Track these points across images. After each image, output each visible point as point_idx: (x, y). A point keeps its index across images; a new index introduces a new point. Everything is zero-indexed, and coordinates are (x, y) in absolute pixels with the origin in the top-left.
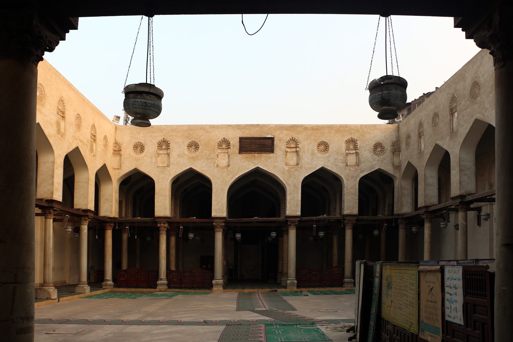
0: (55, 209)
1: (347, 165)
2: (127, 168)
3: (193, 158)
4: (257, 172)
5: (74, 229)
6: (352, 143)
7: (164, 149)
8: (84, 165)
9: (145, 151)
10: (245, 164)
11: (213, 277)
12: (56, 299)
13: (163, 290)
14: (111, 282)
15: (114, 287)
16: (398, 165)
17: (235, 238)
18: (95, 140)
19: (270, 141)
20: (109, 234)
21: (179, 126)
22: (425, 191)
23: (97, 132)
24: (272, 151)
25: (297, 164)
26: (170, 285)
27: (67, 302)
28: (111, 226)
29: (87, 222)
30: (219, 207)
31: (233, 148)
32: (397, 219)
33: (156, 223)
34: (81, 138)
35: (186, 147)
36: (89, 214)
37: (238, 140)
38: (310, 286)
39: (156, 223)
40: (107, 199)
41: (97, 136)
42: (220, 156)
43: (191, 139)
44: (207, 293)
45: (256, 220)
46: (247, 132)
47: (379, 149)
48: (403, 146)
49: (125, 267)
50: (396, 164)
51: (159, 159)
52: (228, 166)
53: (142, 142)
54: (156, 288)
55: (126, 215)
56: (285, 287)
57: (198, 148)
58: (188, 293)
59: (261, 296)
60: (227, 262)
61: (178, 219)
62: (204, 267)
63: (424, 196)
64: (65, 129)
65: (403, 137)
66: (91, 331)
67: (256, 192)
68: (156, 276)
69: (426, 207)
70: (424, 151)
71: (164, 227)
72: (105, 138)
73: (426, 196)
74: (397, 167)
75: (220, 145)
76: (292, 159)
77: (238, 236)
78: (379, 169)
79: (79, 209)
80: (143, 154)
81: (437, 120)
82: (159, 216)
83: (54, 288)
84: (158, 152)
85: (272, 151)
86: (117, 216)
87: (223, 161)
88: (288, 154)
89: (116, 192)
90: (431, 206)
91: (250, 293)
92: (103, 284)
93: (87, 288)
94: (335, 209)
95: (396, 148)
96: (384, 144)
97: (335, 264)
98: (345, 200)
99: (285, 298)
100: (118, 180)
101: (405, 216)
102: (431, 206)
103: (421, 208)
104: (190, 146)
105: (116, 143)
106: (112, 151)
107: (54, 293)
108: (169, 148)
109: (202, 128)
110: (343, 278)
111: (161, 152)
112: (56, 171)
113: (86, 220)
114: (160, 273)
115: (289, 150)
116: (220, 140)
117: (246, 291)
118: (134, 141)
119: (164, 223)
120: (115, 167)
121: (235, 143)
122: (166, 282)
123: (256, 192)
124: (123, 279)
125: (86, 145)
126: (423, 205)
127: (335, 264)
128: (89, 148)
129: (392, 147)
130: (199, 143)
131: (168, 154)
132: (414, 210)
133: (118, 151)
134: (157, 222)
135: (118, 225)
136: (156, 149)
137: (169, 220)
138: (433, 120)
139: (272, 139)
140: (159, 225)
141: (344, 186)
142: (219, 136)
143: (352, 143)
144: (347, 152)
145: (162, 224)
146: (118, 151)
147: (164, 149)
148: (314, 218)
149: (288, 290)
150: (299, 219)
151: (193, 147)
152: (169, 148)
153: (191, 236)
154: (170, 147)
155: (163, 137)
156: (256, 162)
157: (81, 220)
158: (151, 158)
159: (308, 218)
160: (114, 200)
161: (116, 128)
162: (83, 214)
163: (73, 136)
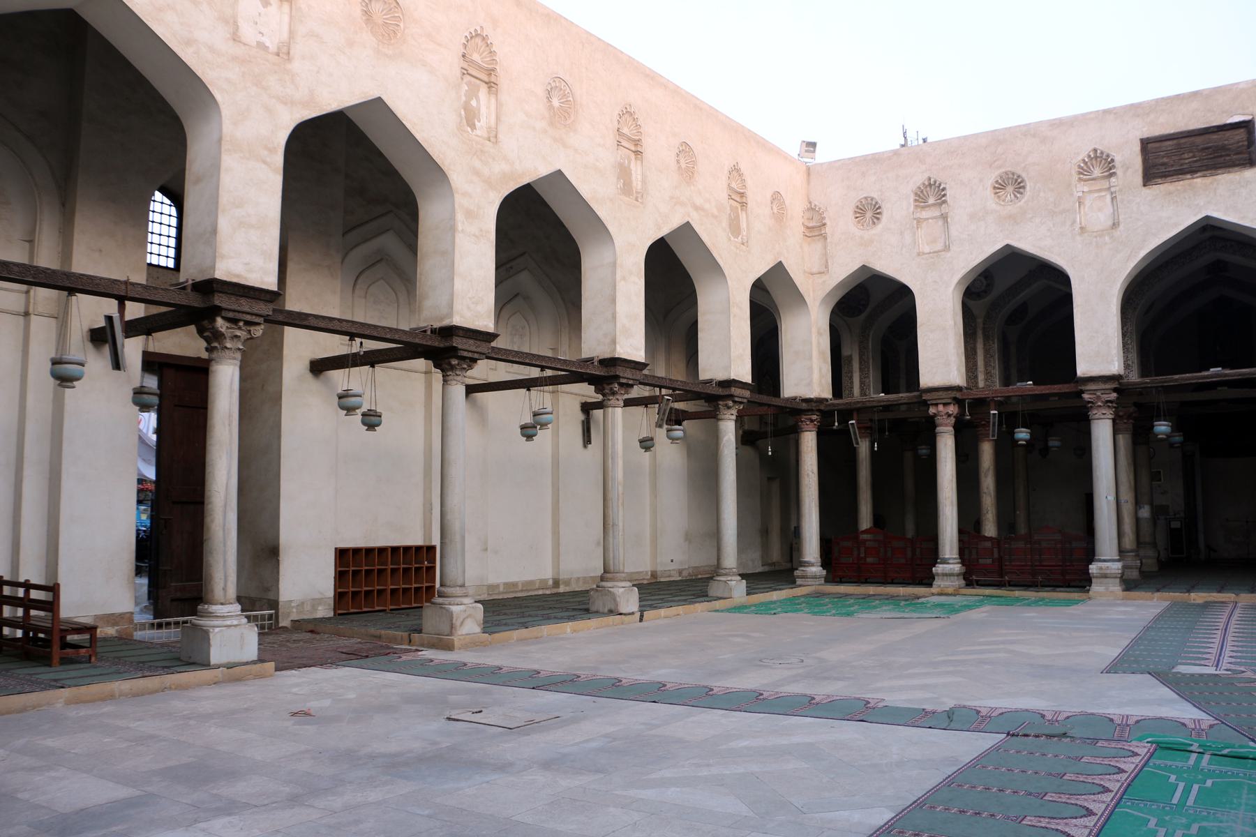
0: (624, 381)
2: (843, 268)
4: (1209, 236)
5: (743, 436)
7: (933, 205)
8: (798, 298)
9: (884, 218)
11: (1090, 554)
12: (633, 613)
13: (950, 590)
14: (817, 570)
15: (828, 580)
18: (744, 205)
19: (1241, 134)
20: (809, 442)
21: (966, 138)
23: (749, 183)
26: (973, 575)
27: (666, 621)
28: (812, 421)
29: (734, 412)
30: (1100, 345)
31: (1125, 173)
33: (926, 404)
34: (699, 201)
35: (989, 192)
36: (735, 391)
39: (926, 404)
41: (749, 194)
42: (1087, 203)
43: (1000, 167)
44: (1069, 603)
45: (1216, 375)
46: (1162, 120)
51: (920, 233)
52: (1115, 225)
53: (875, 195)
54: (930, 585)
55: (863, 393)
57: (1024, 187)
58: (1053, 603)
64: (644, 182)
66: (555, 721)
68: (933, 555)
71: (945, 416)
72: (776, 197)
75: (1084, 171)
79: (709, 382)
80: (880, 227)
84: (918, 215)
86: (827, 393)
87: (1097, 212)
89: (820, 334)
91: (1206, 605)
92: (797, 573)
93: (739, 588)
104: (999, 187)
105: (811, 208)
106: (803, 229)
107: (629, 600)
108: (945, 202)
109: (1029, 132)
111: (925, 214)
112: (621, 287)
113: (729, 408)
114: (941, 542)
116: (1083, 155)
117: (1198, 597)
118: (854, 198)
119: (945, 404)
120: (815, 270)
121: (1130, 160)
122: (957, 568)
125: (715, 217)
128: (725, 224)
130: (1024, 175)
131: (944, 217)
133: (816, 229)
134: (925, 401)
135: (833, 420)
136: (912, 208)
137: (958, 395)
140: (932, 410)
145: (941, 408)
146: (816, 229)
151: (1010, 189)
152: (945, 202)
154: (948, 198)
155: (926, 175)
157: (717, 409)
158: (902, 233)
160: (815, 353)
161: (809, 171)
162: (720, 391)
163: (672, 198)
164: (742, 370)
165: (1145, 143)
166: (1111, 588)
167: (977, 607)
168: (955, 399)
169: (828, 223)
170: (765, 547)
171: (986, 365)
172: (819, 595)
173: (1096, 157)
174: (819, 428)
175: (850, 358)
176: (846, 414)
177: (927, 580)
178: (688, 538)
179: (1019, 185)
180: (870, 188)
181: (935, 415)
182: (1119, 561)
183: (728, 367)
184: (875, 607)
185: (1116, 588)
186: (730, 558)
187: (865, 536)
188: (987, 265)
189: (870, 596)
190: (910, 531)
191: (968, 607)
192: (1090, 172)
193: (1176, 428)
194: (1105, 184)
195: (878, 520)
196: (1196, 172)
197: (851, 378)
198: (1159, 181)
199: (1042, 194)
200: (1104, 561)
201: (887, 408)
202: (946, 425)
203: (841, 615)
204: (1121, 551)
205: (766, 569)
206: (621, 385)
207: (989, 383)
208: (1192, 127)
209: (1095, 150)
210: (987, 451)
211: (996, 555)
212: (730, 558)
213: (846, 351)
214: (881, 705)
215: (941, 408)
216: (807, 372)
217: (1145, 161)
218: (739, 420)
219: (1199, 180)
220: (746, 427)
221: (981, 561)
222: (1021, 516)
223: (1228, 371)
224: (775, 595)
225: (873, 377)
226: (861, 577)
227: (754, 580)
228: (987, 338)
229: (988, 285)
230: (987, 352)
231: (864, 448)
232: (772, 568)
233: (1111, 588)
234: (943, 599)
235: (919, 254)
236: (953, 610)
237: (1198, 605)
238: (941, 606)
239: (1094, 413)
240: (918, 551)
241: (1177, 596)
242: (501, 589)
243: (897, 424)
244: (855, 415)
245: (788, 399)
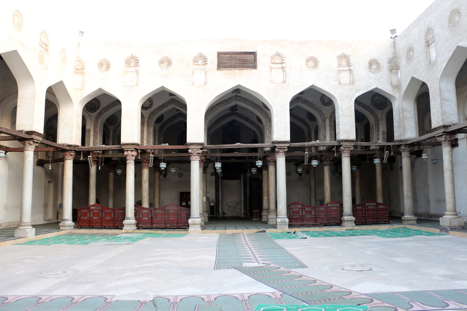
1: (340, 83)
4: (237, 93)
5: (37, 162)
6: (344, 58)
7: (133, 66)
8: (68, 98)
10: (225, 82)
11: (189, 215)
13: (130, 231)
15: (75, 227)
16: (396, 84)
17: (215, 168)
18: (47, 50)
20: (69, 165)
22: (441, 107)
24: (255, 67)
25: (284, 82)
28: (71, 155)
30: (196, 132)
32: (399, 146)
33: (122, 151)
36: (34, 136)
37: (216, 55)
38: (302, 226)
39: (122, 151)
47: (374, 66)
48: (403, 62)
49: (146, 204)
50: (395, 83)
52: (205, 84)
55: (94, 144)
56: (275, 226)
57: (171, 64)
59: (247, 239)
60: (208, 199)
61: (148, 144)
62: (184, 204)
63: (442, 114)
65: (402, 52)
67: (237, 118)
68: (123, 216)
69: (444, 127)
70: (436, 61)
73: (443, 114)
74: (397, 87)
75: (195, 61)
76: (278, 75)
77: (218, 165)
78: (376, 88)
79: (21, 131)
81: (412, 54)
83: (32, 227)
85: (255, 67)
86: (79, 143)
88: (273, 70)
90: (450, 126)
91: (233, 235)
92: (60, 224)
93: (31, 232)
94: (325, 136)
95: (394, 66)
96: (379, 61)
97: (327, 199)
98: (341, 123)
99: (280, 242)
100: (81, 102)
101: (409, 142)
102: (450, 126)
103: (436, 129)
104: (161, 62)
106: (74, 69)
108: (138, 65)
110: (342, 215)
113: (31, 145)
115: (272, 65)
117: (230, 231)
119: (131, 151)
121: (213, 60)
122: (134, 221)
123: (237, 118)
124: (86, 218)
126: (441, 124)
127: (327, 199)
129: (389, 64)
130: (172, 59)
131: (137, 72)
132: (418, 135)
133: (80, 70)
134: (123, 149)
137: (137, 147)
138: (450, 20)
139: (254, 54)
141: (338, 107)
143: (344, 58)
144: (339, 68)
145: (129, 152)
146: (80, 70)
147: (133, 66)
148: (306, 144)
149: (279, 230)
150: (288, 145)
151: (165, 64)
153: (163, 165)
157: (24, 144)
159: (299, 144)
162: (27, 136)
164: (40, 128)
165: (219, 54)
166: (197, 229)
167: (144, 238)
168: (136, 149)
170: (45, 213)
171: (148, 137)
172: (71, 234)
173: (200, 56)
174: (74, 158)
175: (89, 130)
176: (87, 153)
177: (120, 227)
178: (6, 208)
179: (169, 63)
181: (127, 155)
182: (200, 218)
184: (98, 240)
185: (199, 229)
186: (27, 217)
187: (92, 208)
188: (150, 96)
189: (95, 234)
190: (111, 205)
191: (140, 239)
192: (198, 62)
193: (222, 168)
194: (203, 67)
195: (97, 201)
196: (236, 68)
197: (89, 139)
198: (223, 69)
200: (194, 218)
201: (104, 152)
202: (131, 160)
203: (83, 244)
205: (46, 222)
206: (34, 142)
207: (148, 144)
209: (200, 54)
210: (146, 173)
211: (150, 216)
212: (27, 217)
213: (88, 127)
214: (114, 299)
215: (129, 152)
216: (70, 132)
217: (218, 60)
218: (36, 152)
219: (237, 71)
220: (39, 158)
221: (144, 218)
222: (157, 199)
223: (242, 144)
224: (50, 235)
225: (99, 138)
226: (90, 225)
227: (38, 227)
228: (148, 126)
229: (151, 105)
230: (148, 132)
231: (93, 170)
232: (49, 222)
233: (197, 229)
234: (127, 235)
235: (125, 86)
236: (134, 240)
237: (230, 235)
238: (128, 238)
239: (192, 158)
240: (116, 214)
241: (222, 231)
243: (108, 161)
244: (91, 153)
245: (60, 145)
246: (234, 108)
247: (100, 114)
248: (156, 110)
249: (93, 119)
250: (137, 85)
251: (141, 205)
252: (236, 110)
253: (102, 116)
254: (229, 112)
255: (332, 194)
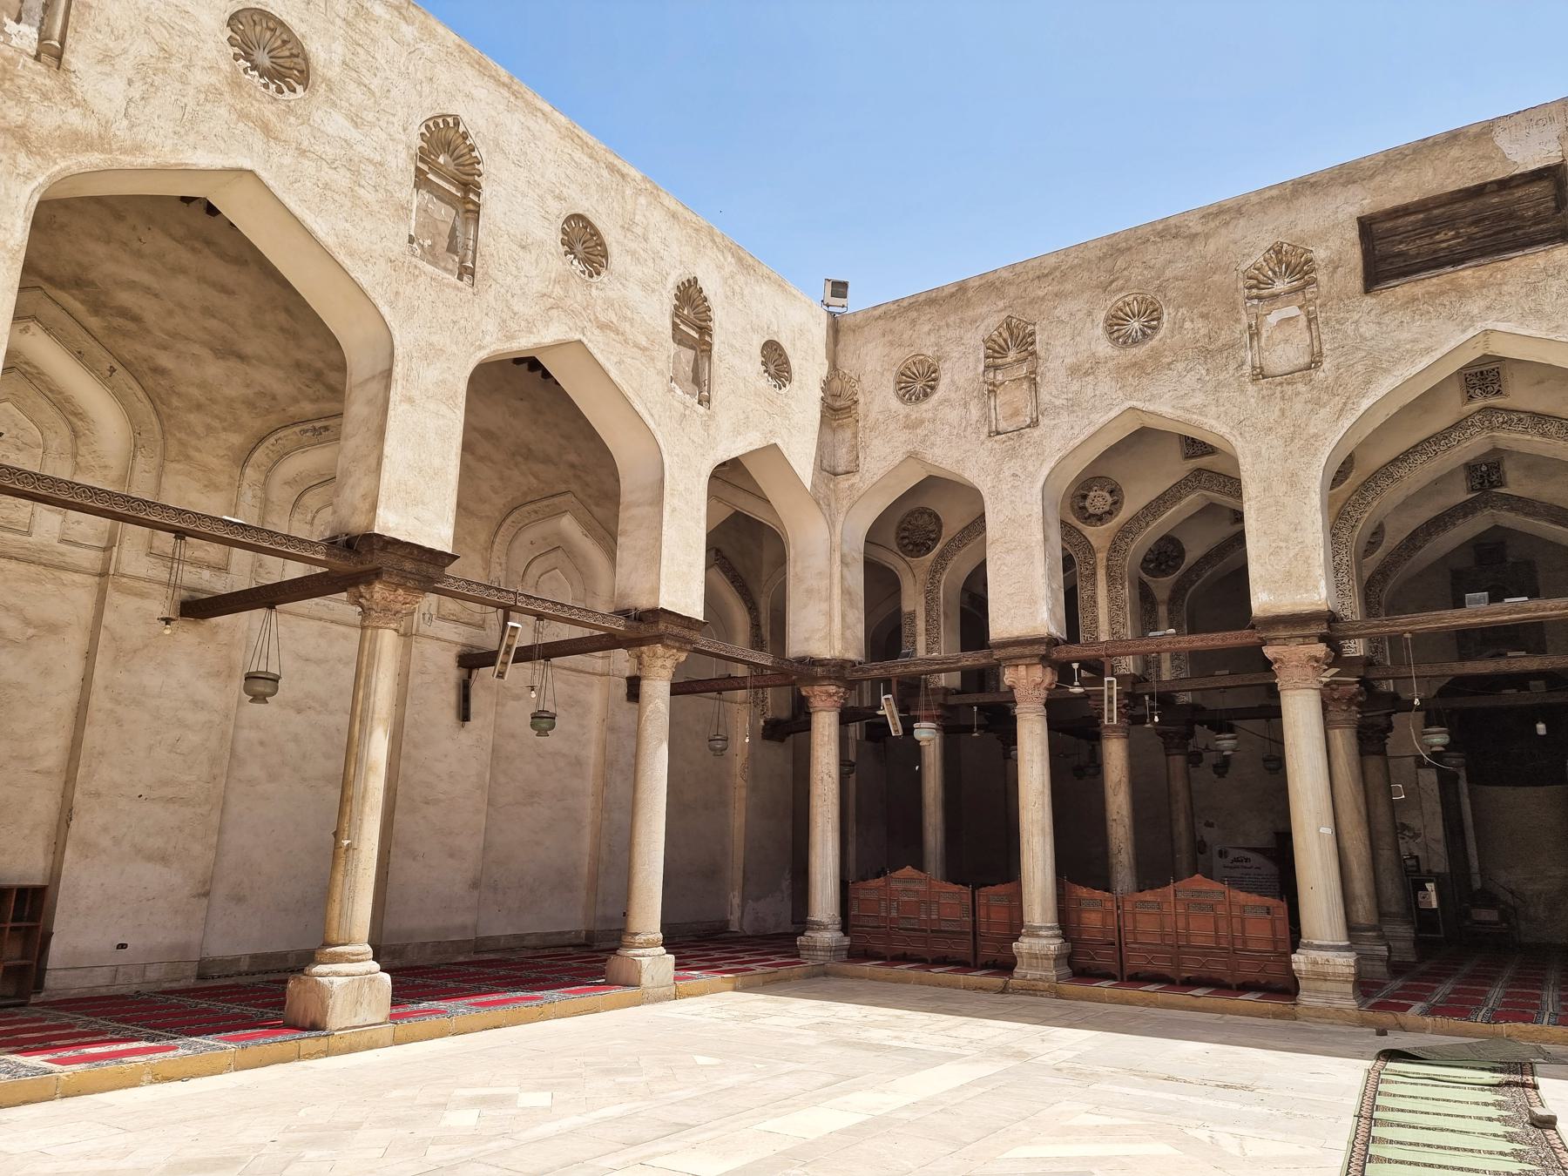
3: (1135, 364)
29: (669, 663)
37: (1353, 234)
40: (809, 591)
82: (1006, 635)
92: (800, 940)
125: (644, 349)
131: (1033, 382)
136: (981, 368)
142: (1253, 244)
152: (1033, 353)
154: (1038, 347)
156: (1474, 306)
158: (966, 405)
169: (861, 401)
180: (924, 340)
182: (1347, 949)
183: (655, 591)
196: (1462, 261)
199: (1188, 325)
204: (1351, 928)
208: (1452, 187)
229: (1115, 503)
242: (244, 967)
246: (1485, 474)
247: (943, 557)
248: (1135, 518)
249: (922, 576)
250: (1035, 423)
251: (281, 1005)
252: (1501, 484)
253: (950, 566)
254: (1461, 495)
255: (1457, 794)
